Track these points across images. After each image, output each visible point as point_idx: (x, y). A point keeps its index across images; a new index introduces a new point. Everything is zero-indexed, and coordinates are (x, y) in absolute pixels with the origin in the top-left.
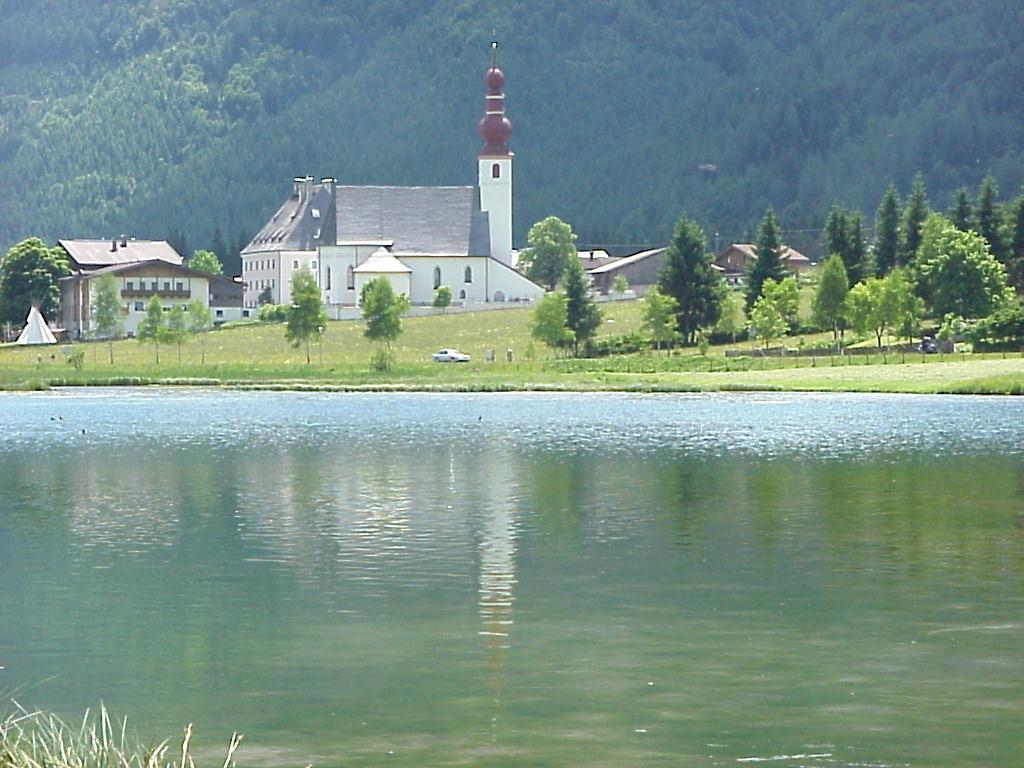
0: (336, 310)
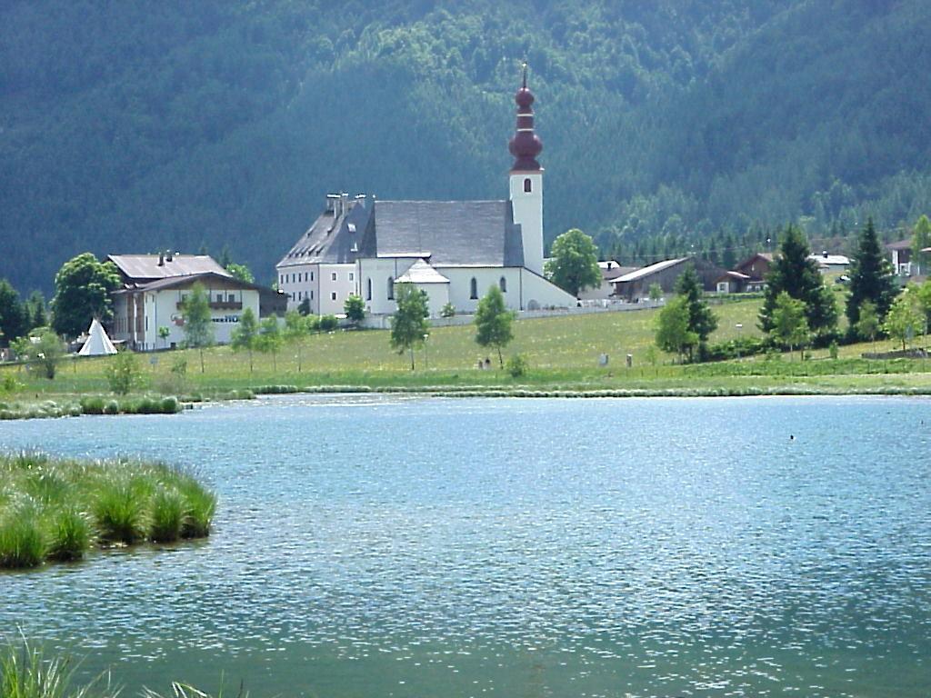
0: (381, 319)
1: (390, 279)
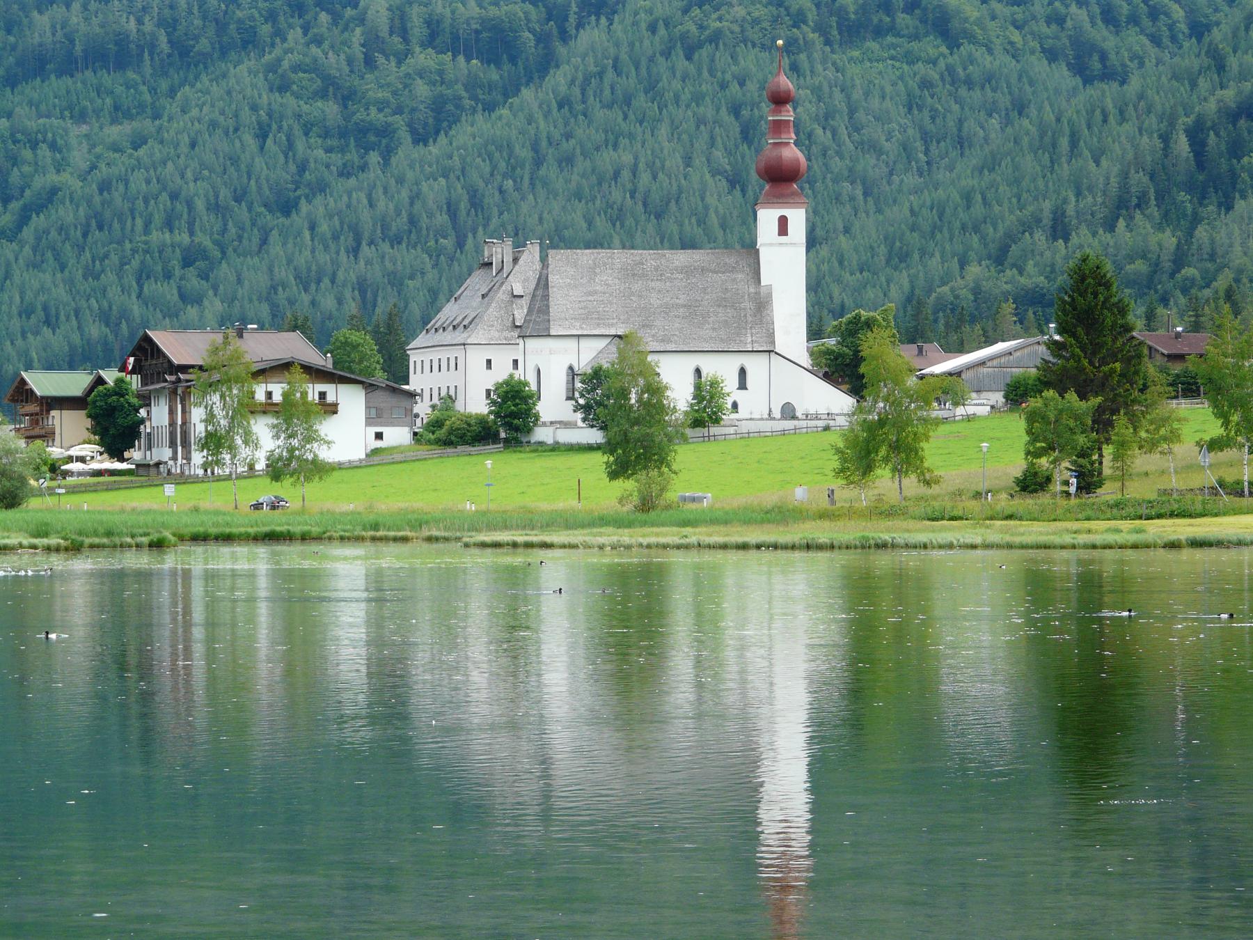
1: (571, 368)
